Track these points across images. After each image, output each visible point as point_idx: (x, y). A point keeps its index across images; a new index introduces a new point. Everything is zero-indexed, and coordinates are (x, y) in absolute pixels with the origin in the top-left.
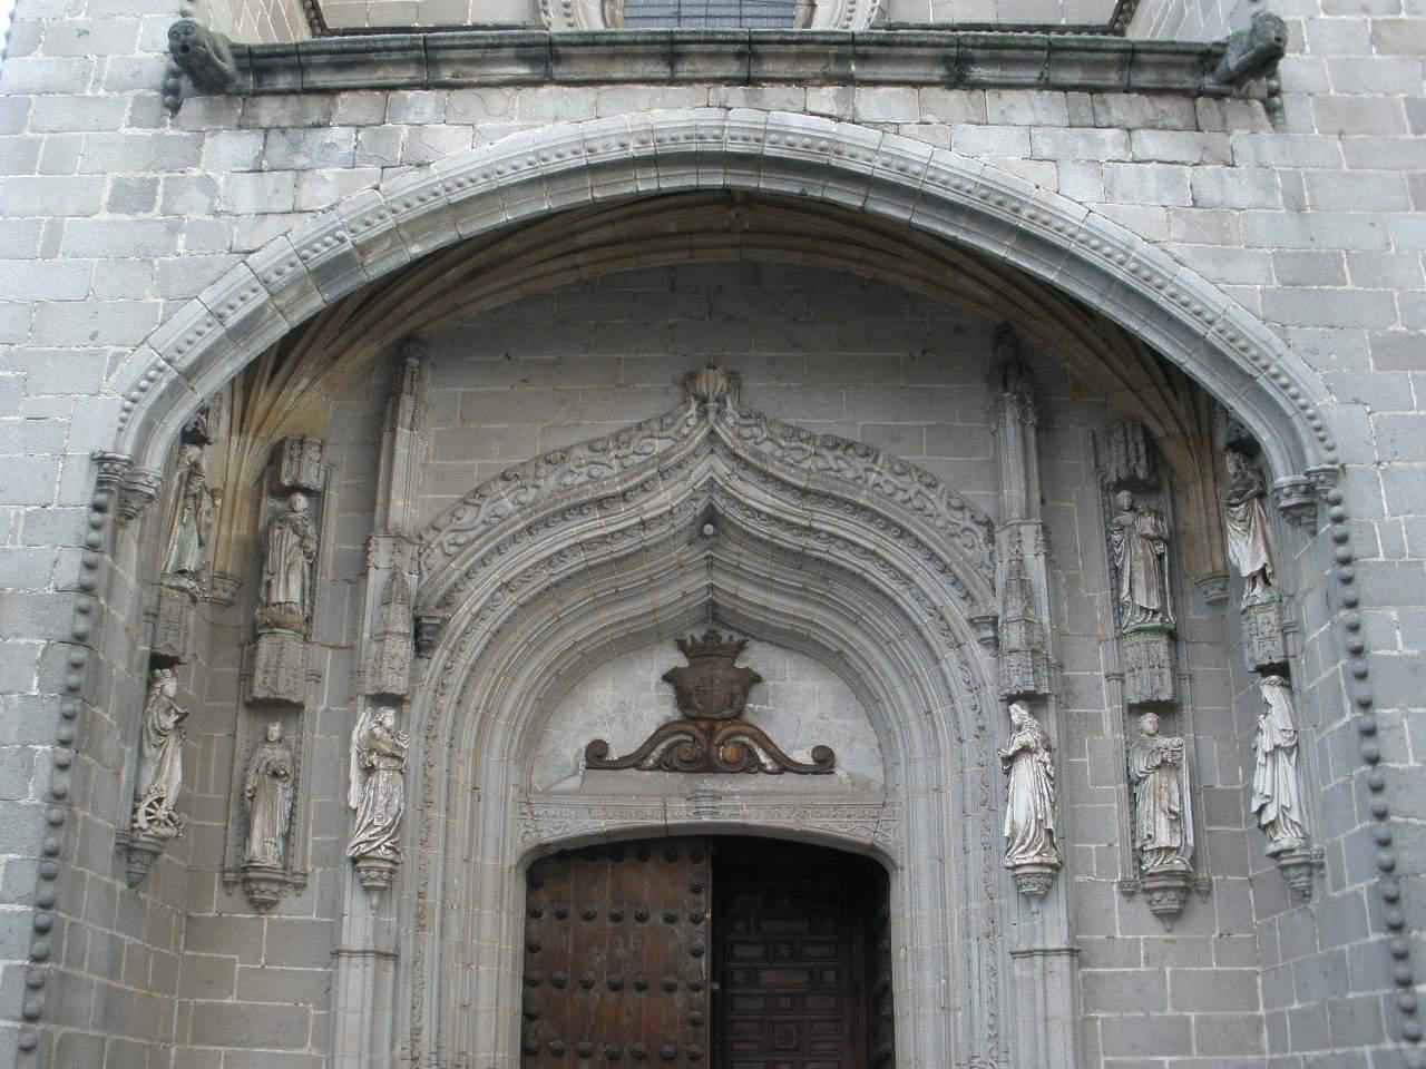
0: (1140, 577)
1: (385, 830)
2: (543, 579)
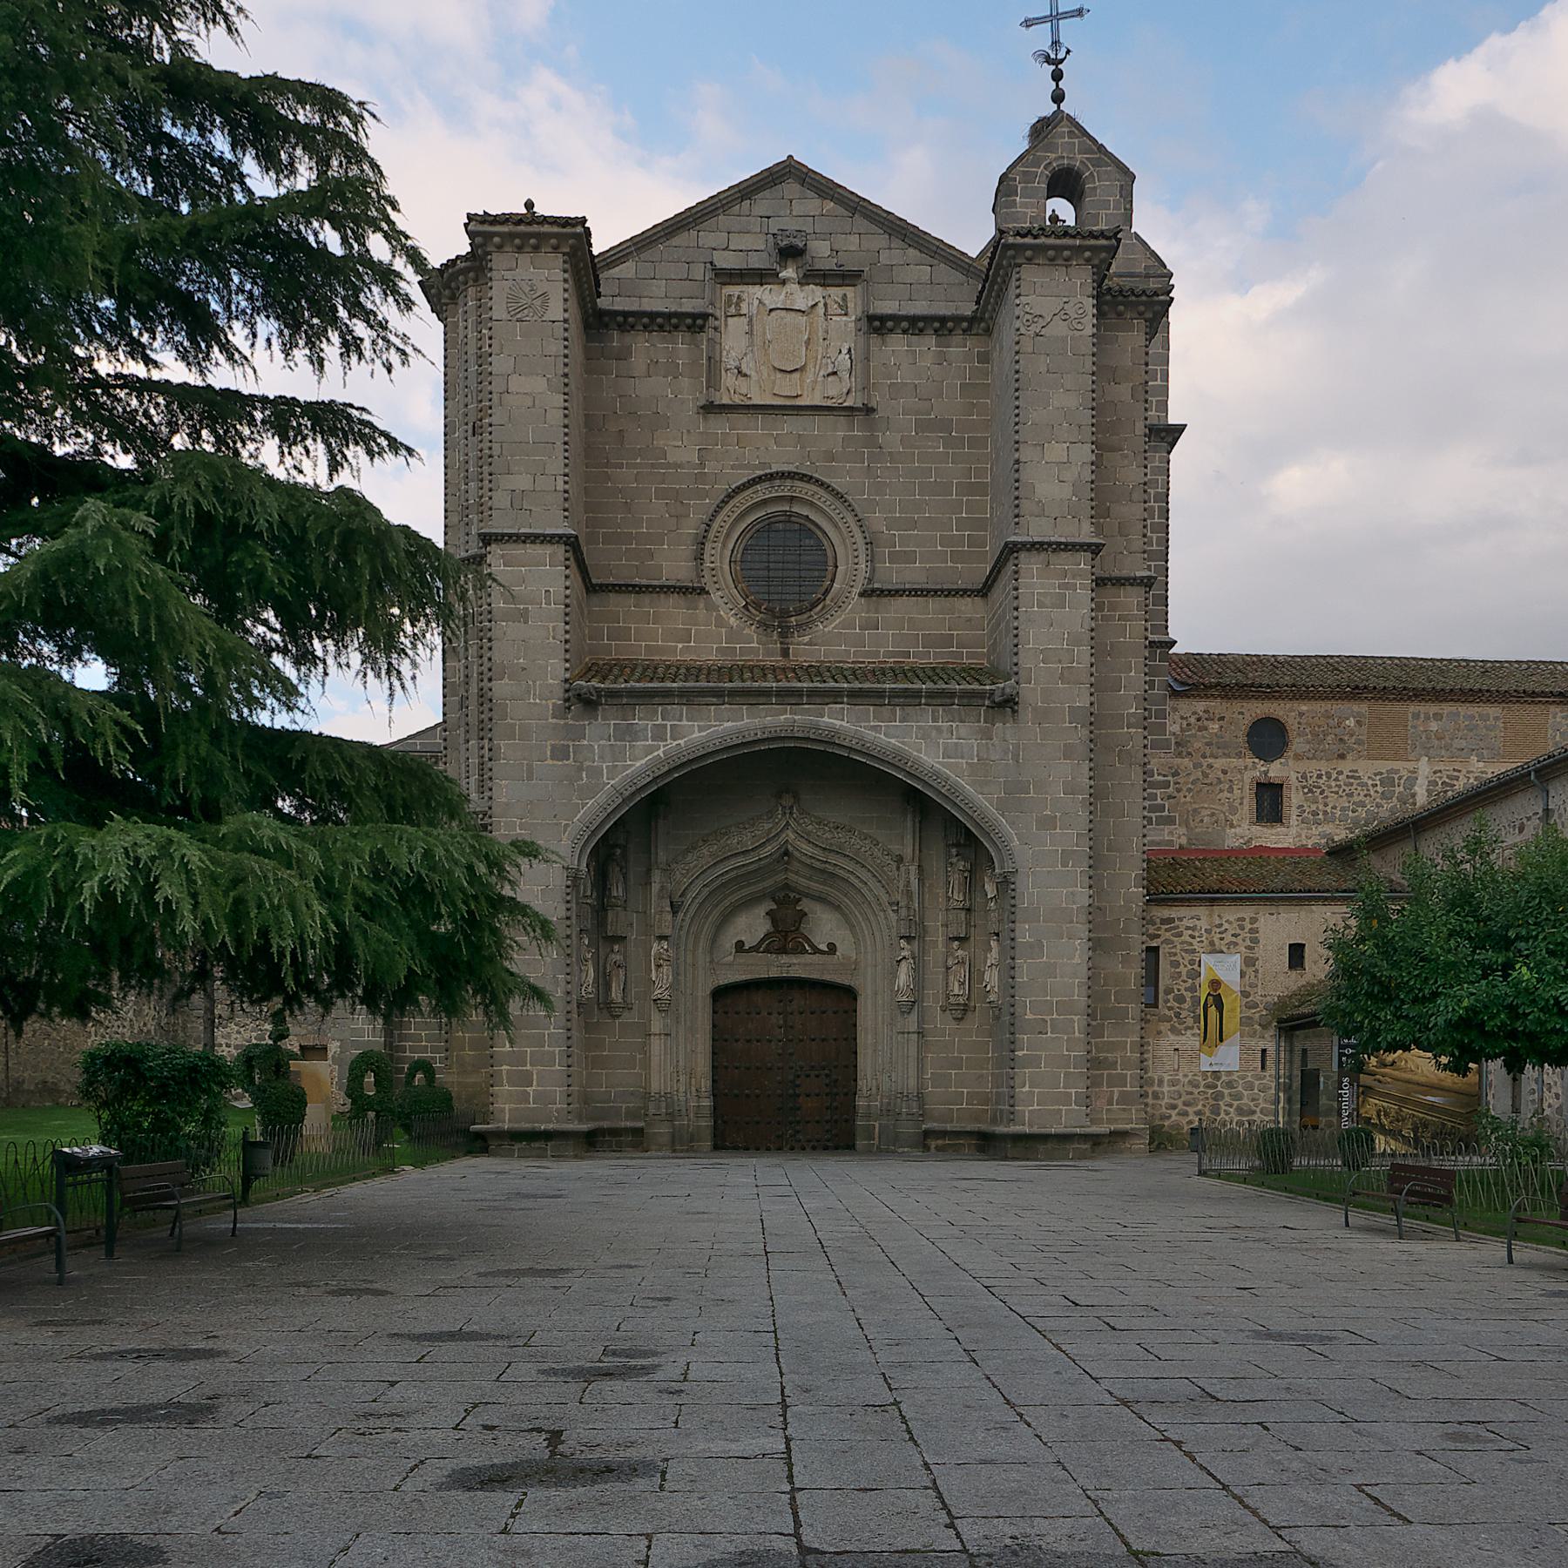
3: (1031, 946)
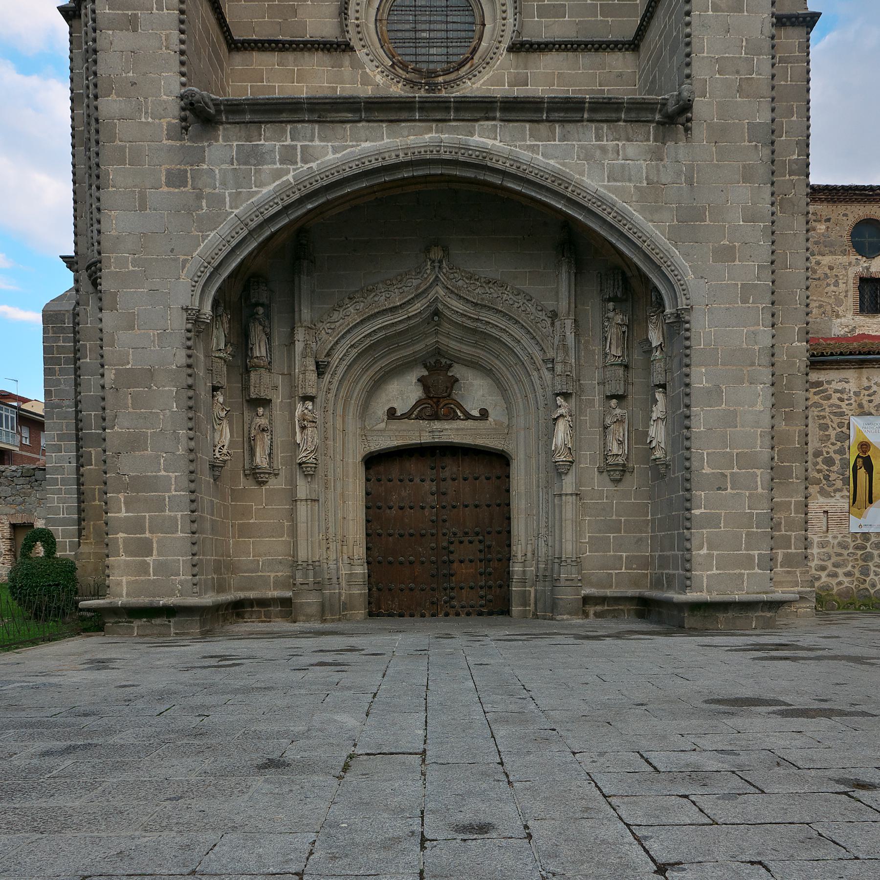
0: (614, 342)
1: (311, 452)
2: (368, 342)
3: (709, 392)
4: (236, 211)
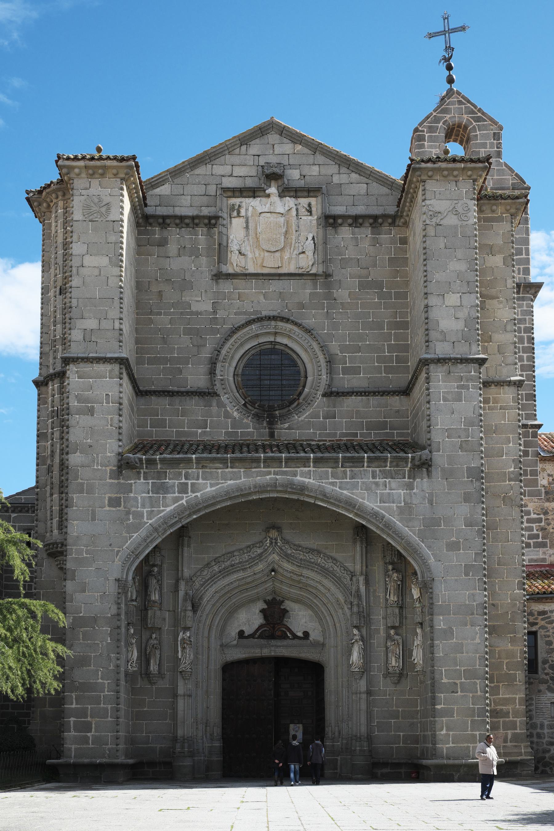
0: (392, 591)
1: (189, 664)
3: (445, 631)
4: (150, 522)
